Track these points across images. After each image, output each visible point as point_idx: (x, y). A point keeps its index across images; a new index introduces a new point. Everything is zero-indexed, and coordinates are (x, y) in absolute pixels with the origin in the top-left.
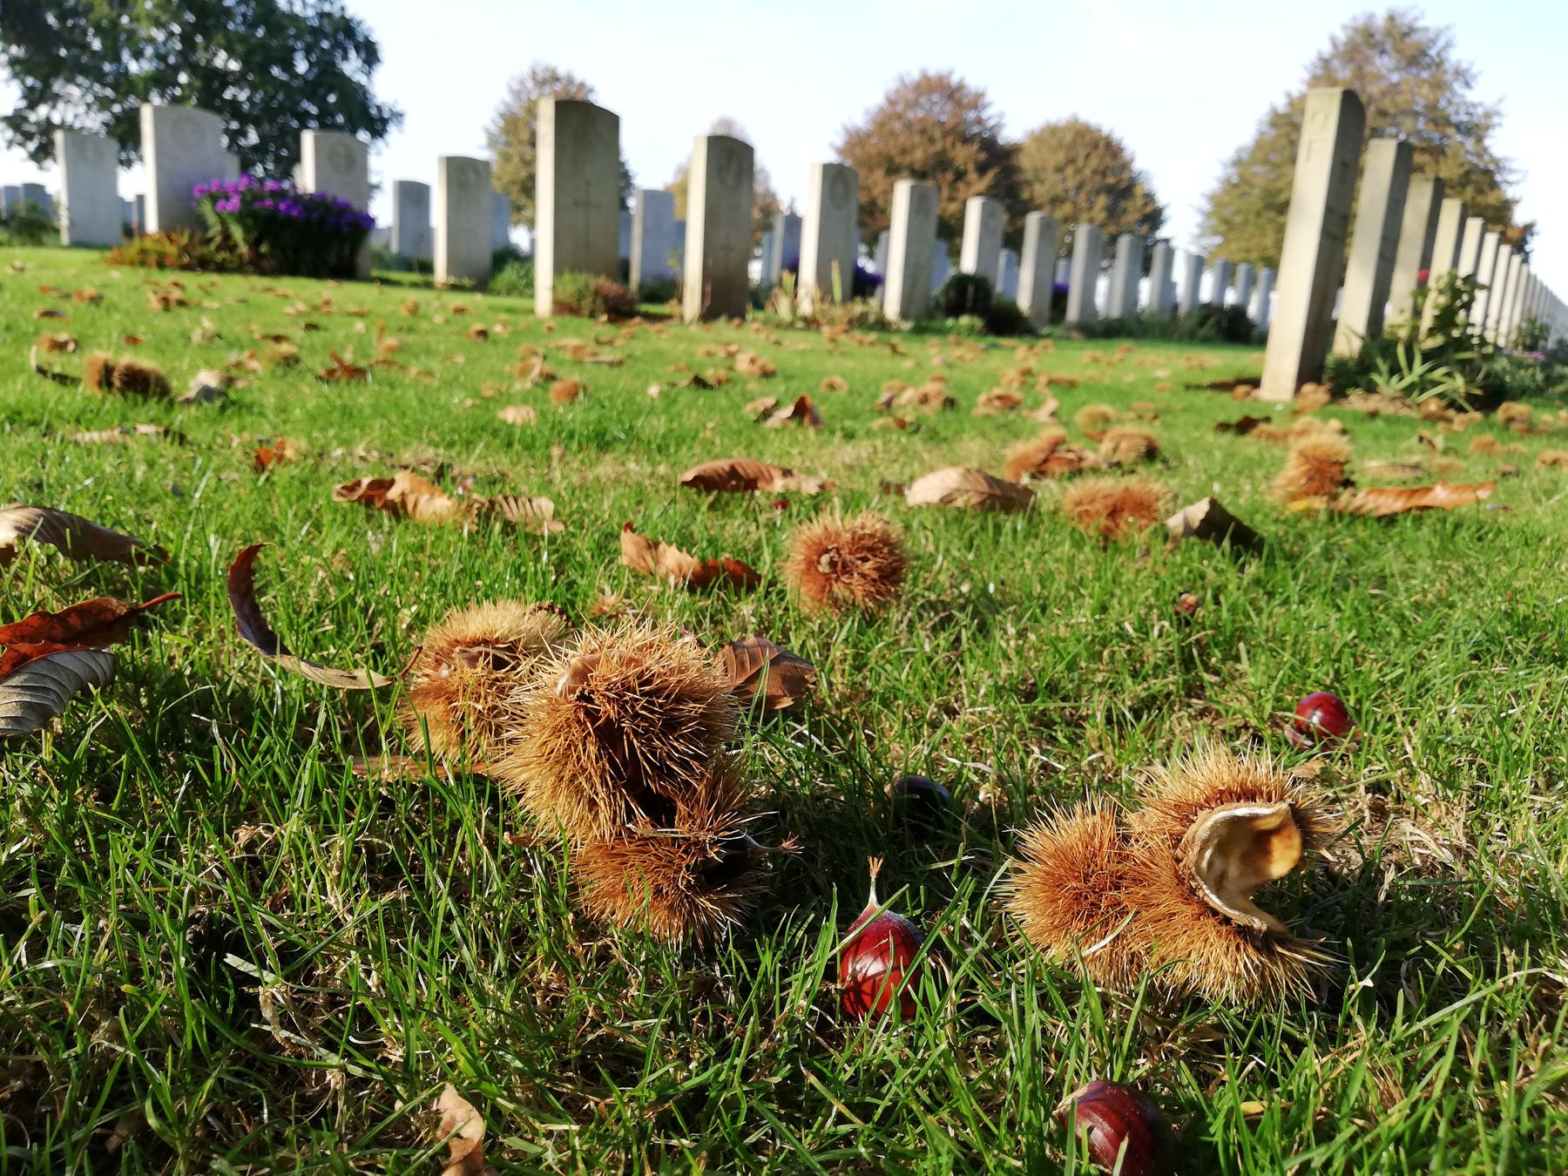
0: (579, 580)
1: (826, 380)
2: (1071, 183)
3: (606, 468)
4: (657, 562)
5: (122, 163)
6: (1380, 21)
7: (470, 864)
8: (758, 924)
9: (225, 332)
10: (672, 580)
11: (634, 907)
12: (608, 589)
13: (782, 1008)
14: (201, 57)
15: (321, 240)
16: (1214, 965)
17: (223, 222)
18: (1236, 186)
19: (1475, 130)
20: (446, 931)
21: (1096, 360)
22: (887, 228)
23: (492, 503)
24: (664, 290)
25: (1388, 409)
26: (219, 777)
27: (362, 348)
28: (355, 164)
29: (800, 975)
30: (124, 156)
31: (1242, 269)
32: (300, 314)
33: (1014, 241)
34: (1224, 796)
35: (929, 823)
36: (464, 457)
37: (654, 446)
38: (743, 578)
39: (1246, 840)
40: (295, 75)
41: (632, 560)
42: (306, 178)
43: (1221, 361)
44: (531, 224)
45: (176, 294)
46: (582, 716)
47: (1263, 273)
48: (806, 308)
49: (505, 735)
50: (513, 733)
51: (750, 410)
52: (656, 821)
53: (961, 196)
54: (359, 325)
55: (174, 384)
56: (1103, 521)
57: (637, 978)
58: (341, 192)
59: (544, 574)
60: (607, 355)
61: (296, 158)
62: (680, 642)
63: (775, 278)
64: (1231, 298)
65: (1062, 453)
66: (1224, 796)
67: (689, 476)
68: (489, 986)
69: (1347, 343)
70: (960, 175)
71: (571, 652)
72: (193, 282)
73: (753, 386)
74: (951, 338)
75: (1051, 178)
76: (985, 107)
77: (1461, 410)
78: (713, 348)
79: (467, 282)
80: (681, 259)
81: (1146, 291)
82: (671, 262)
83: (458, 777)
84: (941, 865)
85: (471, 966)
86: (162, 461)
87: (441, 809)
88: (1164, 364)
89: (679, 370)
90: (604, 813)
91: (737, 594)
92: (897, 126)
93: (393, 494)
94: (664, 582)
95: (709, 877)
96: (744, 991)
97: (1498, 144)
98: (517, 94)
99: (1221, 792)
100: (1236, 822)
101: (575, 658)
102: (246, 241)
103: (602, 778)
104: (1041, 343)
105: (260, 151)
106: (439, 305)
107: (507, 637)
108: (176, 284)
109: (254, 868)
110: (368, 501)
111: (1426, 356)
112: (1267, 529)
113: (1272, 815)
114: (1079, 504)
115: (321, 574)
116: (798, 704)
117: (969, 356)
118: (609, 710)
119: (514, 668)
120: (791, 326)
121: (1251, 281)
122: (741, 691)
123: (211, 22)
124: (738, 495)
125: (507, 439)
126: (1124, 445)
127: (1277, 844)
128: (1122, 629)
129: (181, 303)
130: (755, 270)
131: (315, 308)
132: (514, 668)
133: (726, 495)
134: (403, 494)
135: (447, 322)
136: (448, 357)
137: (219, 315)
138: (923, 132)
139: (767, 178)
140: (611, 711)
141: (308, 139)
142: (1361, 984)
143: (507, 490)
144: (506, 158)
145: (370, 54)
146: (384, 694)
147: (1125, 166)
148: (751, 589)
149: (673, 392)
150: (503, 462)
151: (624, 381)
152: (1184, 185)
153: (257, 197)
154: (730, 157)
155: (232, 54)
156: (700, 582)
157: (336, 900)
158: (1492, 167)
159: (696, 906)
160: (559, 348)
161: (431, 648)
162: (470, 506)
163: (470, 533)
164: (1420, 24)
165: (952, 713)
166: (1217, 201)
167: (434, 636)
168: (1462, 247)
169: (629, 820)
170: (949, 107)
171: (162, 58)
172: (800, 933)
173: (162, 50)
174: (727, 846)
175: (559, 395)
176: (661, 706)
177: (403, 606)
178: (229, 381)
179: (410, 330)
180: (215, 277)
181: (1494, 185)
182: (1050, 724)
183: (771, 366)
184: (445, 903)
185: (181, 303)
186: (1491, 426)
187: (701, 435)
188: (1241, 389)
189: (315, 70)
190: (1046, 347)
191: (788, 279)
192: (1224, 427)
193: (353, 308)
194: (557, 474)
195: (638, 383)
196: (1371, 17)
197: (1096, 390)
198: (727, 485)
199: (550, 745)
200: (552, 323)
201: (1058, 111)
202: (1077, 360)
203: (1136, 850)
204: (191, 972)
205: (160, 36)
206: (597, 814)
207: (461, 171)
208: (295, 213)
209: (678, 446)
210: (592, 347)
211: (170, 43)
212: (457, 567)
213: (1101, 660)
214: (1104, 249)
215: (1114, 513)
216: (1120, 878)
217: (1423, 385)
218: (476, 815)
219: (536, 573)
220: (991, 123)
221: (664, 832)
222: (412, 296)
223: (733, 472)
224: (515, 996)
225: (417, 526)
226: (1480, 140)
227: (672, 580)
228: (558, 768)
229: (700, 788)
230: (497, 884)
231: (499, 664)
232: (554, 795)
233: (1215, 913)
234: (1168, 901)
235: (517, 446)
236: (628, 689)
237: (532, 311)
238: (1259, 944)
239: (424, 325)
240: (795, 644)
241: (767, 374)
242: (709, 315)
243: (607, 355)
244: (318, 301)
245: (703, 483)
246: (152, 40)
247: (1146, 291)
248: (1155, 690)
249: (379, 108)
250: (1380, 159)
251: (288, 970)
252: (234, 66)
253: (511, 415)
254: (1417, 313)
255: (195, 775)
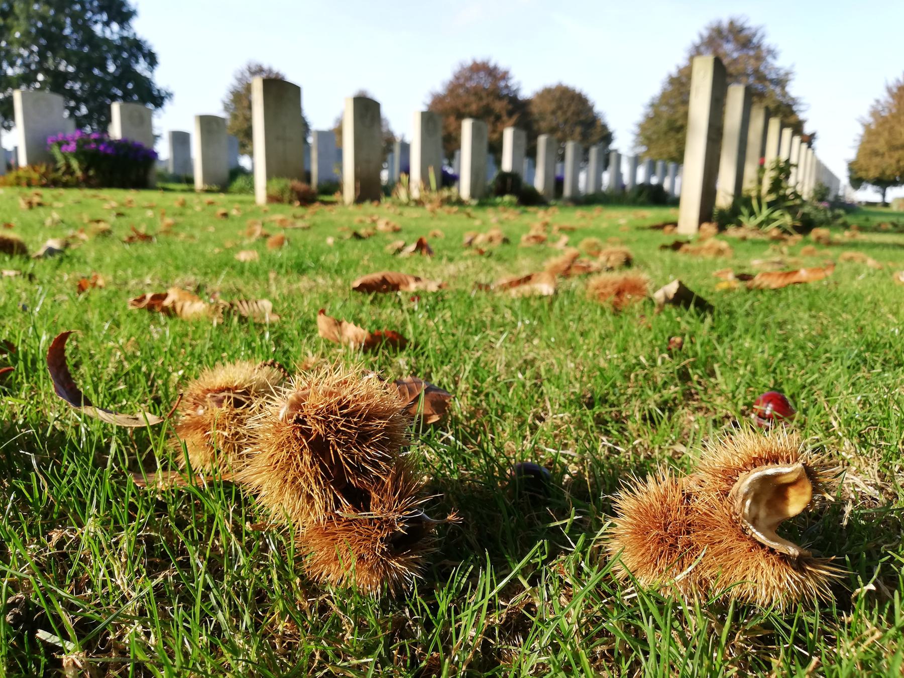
0: (291, 349)
1: (431, 233)
2: (561, 120)
3: (304, 283)
4: (341, 333)
5: (5, 128)
6: (725, 24)
7: (222, 546)
8: (434, 576)
9: (66, 219)
10: (352, 345)
11: (346, 571)
12: (310, 354)
13: (457, 638)
14: (50, 64)
15: (127, 166)
16: (766, 582)
17: (66, 158)
18: (652, 118)
19: (781, 82)
20: (205, 597)
21: (583, 217)
22: (459, 147)
23: (232, 305)
24: (332, 187)
25: (751, 236)
26: (37, 496)
27: (151, 223)
28: (145, 122)
29: (469, 612)
30: (6, 124)
31: (659, 165)
32: (113, 208)
33: (532, 153)
34: (756, 462)
35: (540, 494)
36: (214, 281)
37: (333, 271)
38: (397, 342)
39: (772, 492)
40: (109, 74)
41: (325, 334)
42: (116, 131)
43: (653, 214)
44: (251, 154)
45: (36, 199)
46: (298, 434)
47: (671, 166)
48: (416, 194)
49: (244, 452)
50: (249, 450)
51: (389, 249)
52: (357, 507)
53: (499, 129)
54: (150, 213)
55: (30, 247)
56: (613, 298)
57: (348, 624)
58: (136, 138)
59: (267, 347)
60: (300, 224)
61: (109, 120)
62: (366, 378)
63: (396, 178)
64: (654, 181)
65: (578, 263)
66: (756, 462)
67: (357, 284)
68: (239, 641)
69: (724, 199)
70: (498, 118)
71: (288, 390)
72: (47, 194)
73: (390, 237)
74: (500, 208)
75: (549, 117)
76: (509, 79)
77: (790, 234)
78: (363, 218)
79: (215, 188)
80: (341, 168)
81: (607, 178)
82: (336, 171)
83: (211, 484)
84: (558, 523)
85: (224, 625)
86: (18, 291)
87: (199, 507)
88: (622, 217)
89: (344, 230)
90: (319, 504)
91: (395, 351)
92: (461, 91)
93: (167, 302)
94: (347, 346)
95: (398, 545)
96: (428, 626)
97: (794, 90)
98: (240, 80)
99: (755, 459)
100: (765, 479)
101: (291, 394)
102: (80, 169)
103: (316, 478)
104: (551, 210)
105: (88, 118)
106: (197, 201)
107: (243, 385)
108: (37, 194)
109: (60, 564)
110: (150, 308)
111: (770, 205)
112: (711, 300)
113: (792, 472)
114: (597, 288)
115: (119, 353)
116: (444, 419)
117: (512, 217)
118: (318, 429)
119: (248, 406)
120: (407, 205)
121: (665, 172)
122: (407, 411)
123: (56, 44)
124: (388, 294)
125: (241, 269)
126: (612, 258)
127: (792, 493)
128: (639, 360)
129: (40, 204)
130: (385, 175)
131: (122, 205)
132: (248, 406)
133: (380, 295)
134: (174, 302)
135: (203, 210)
136: (204, 228)
137: (63, 210)
138: (476, 94)
139: (387, 125)
140: (319, 429)
141: (116, 108)
142: (866, 588)
143: (242, 297)
144: (235, 117)
145: (152, 60)
146: (157, 429)
147: (590, 109)
148: (403, 348)
149: (342, 242)
150: (240, 283)
151: (311, 238)
152: (623, 119)
153: (87, 143)
154: (366, 109)
155: (69, 62)
156: (371, 345)
157: (121, 579)
158: (791, 103)
159: (389, 566)
160: (271, 221)
161: (191, 395)
162: (217, 307)
163: (218, 325)
164: (747, 25)
165: (542, 419)
166: (643, 127)
167: (194, 388)
168: (781, 145)
169: (337, 508)
170: (490, 79)
171: (26, 65)
172: (464, 580)
173: (27, 62)
174: (410, 521)
175: (273, 244)
176: (356, 423)
177: (174, 371)
178: (67, 245)
179: (181, 214)
180: (62, 191)
181: (792, 113)
182: (606, 422)
183: (398, 226)
184: (202, 577)
185: (40, 204)
186: (809, 242)
187: (361, 263)
188: (668, 228)
189: (120, 70)
190: (554, 212)
191: (404, 178)
192: (664, 247)
193: (146, 204)
194: (273, 288)
195: (320, 238)
196: (720, 22)
197: (586, 232)
198: (381, 288)
199: (276, 457)
200: (267, 208)
201: (551, 80)
202: (576, 217)
203: (696, 504)
204: (12, 645)
205: (25, 53)
206: (313, 504)
207: (208, 123)
208: (109, 151)
209: (348, 270)
210: (291, 220)
211: (32, 57)
212: (209, 345)
213: (629, 379)
214: (583, 157)
215: (619, 293)
216: (689, 525)
217: (768, 221)
218: (225, 507)
219: (262, 346)
220: (514, 88)
221: (363, 515)
222: (181, 196)
223: (384, 281)
224: (260, 647)
225: (182, 321)
226: (783, 87)
227: (352, 345)
228: (283, 473)
229: (387, 481)
230: (243, 560)
231: (238, 403)
232: (281, 493)
233: (763, 546)
234: (728, 540)
235: (247, 274)
236: (331, 413)
237: (254, 202)
238: (795, 565)
239: (189, 212)
240: (435, 380)
241: (396, 231)
242: (360, 199)
243: (300, 224)
244: (124, 201)
245: (366, 288)
246: (20, 56)
247: (607, 178)
248: (666, 397)
249: (159, 91)
250: (736, 96)
251: (83, 641)
252: (71, 69)
253: (243, 256)
254: (760, 182)
255: (19, 493)
